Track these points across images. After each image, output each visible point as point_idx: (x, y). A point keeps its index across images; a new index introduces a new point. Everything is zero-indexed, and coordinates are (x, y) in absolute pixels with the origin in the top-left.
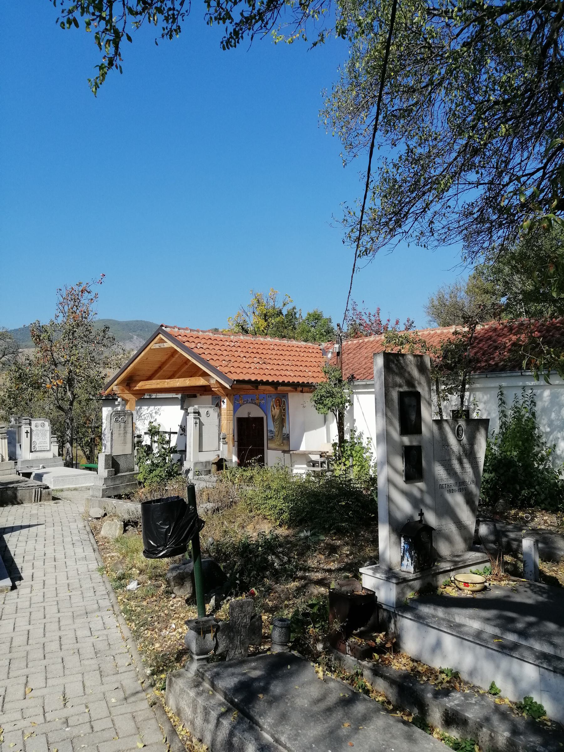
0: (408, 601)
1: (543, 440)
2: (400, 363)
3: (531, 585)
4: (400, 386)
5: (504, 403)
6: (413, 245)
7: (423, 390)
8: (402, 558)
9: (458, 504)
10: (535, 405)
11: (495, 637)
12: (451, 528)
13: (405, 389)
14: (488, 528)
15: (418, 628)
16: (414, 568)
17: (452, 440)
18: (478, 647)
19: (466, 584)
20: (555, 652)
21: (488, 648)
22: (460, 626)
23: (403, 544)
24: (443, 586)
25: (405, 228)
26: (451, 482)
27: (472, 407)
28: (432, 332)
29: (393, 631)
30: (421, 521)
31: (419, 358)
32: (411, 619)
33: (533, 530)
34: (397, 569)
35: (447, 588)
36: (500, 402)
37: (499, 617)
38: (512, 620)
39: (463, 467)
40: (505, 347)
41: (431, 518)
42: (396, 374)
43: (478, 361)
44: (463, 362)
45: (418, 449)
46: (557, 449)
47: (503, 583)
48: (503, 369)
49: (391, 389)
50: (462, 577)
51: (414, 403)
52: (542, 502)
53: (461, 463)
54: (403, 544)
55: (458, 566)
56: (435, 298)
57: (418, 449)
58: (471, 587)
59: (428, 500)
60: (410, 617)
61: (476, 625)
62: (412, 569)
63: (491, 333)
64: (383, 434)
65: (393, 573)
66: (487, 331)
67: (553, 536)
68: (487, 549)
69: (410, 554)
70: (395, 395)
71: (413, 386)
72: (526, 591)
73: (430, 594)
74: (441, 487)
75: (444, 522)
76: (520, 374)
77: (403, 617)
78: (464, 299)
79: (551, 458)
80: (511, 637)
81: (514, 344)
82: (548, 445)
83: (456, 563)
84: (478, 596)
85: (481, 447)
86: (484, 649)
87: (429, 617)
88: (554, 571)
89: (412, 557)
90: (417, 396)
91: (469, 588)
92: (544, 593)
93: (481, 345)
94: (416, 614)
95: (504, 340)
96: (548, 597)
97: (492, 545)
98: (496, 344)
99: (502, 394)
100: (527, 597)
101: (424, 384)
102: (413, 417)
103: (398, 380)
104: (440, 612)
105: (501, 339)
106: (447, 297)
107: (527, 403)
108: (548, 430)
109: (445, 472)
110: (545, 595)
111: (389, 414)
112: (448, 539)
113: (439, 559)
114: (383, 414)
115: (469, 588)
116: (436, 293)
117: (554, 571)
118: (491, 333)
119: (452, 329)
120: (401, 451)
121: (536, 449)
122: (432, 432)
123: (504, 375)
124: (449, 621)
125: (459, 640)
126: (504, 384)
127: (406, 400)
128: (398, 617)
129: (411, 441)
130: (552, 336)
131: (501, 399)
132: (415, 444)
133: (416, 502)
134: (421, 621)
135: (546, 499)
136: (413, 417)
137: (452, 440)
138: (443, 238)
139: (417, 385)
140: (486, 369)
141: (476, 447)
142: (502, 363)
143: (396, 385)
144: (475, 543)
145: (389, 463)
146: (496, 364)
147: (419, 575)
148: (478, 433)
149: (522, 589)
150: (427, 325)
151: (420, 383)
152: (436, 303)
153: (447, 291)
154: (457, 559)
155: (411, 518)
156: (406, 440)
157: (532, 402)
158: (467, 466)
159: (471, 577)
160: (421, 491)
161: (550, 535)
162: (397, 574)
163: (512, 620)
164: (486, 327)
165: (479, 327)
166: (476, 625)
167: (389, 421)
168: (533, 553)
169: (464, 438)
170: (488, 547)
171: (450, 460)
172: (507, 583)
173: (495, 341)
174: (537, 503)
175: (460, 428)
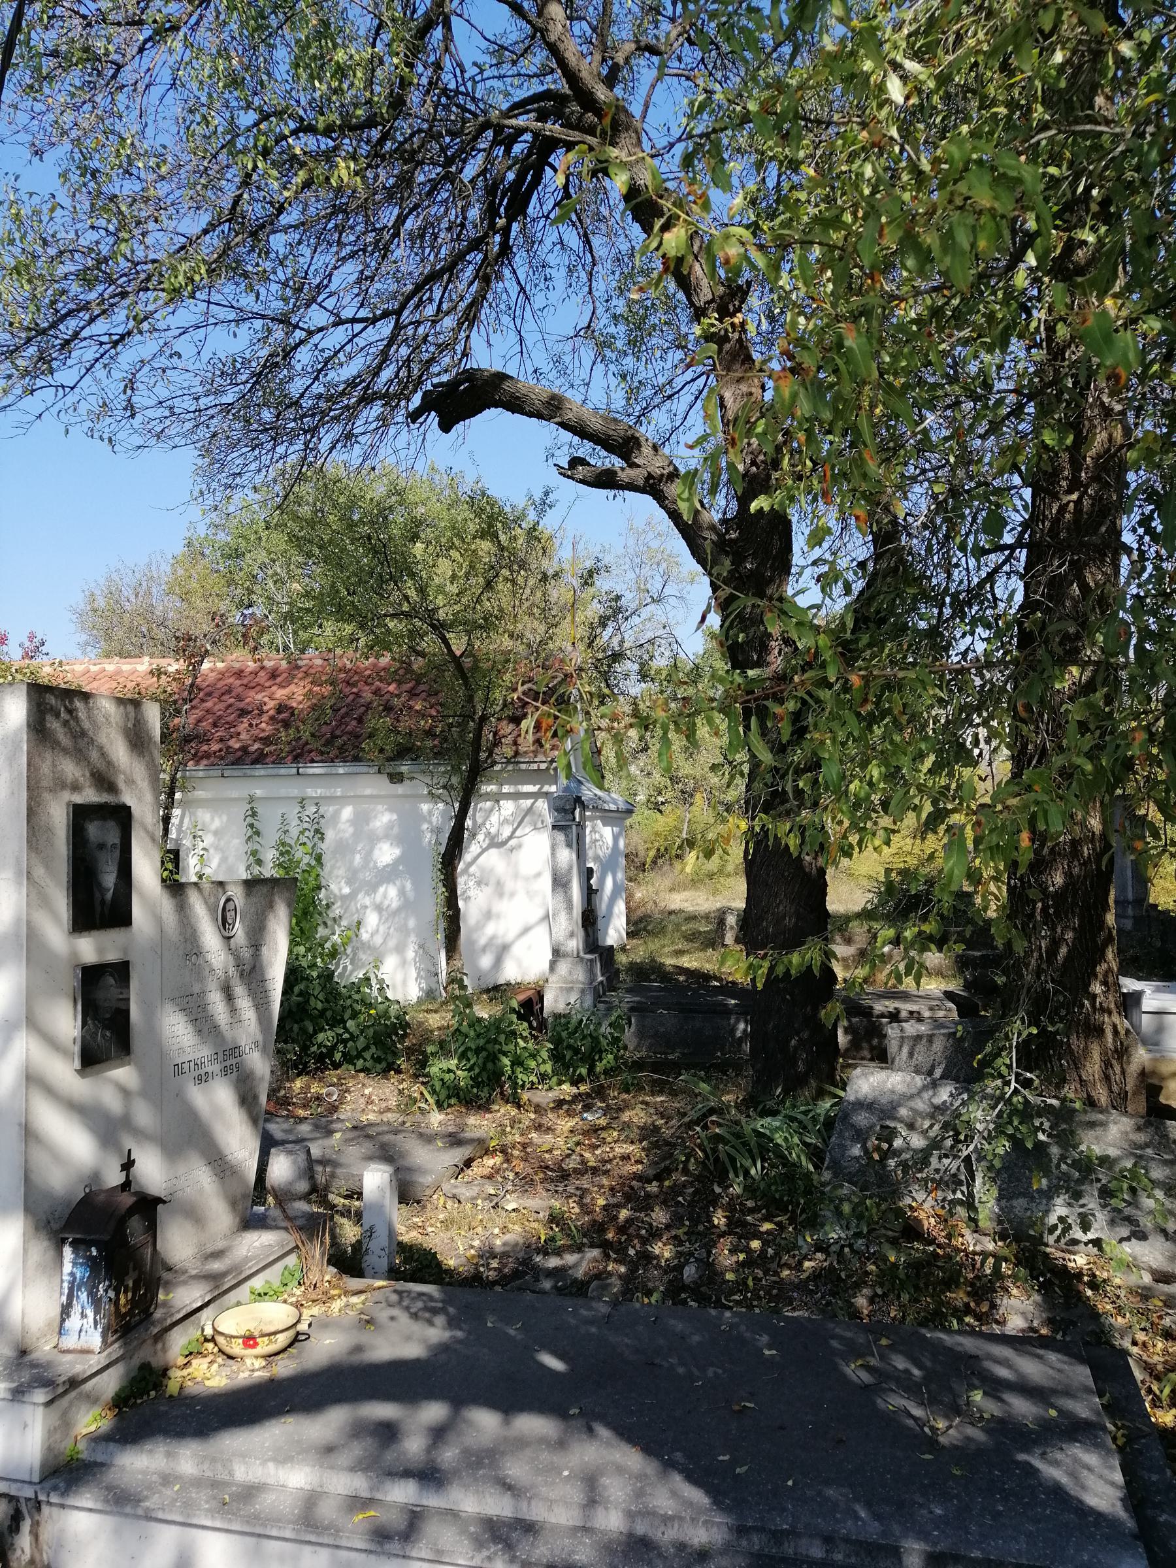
0: (82, 1446)
1: (336, 911)
2: (77, 719)
3: (399, 1293)
4: (76, 788)
5: (258, 833)
6: (77, 432)
7: (140, 799)
8: (66, 1311)
9: (217, 1111)
10: (322, 839)
11: (357, 1503)
12: (200, 1181)
13: (90, 796)
14: (295, 1162)
15: (117, 1532)
16: (104, 1335)
17: (210, 938)
18: (308, 1549)
19: (250, 1340)
20: (516, 1509)
21: (337, 1547)
22: (250, 1492)
23: (68, 1267)
24: (181, 1361)
25: (65, 376)
26: (205, 1052)
27: (187, 842)
28: (94, 669)
29: (26, 1557)
30: (126, 1185)
31: (130, 708)
32: (90, 1510)
33: (355, 1128)
34: (44, 1349)
35: (195, 1362)
36: (250, 833)
37: (359, 1430)
38: (388, 1433)
39: (233, 1010)
40: (261, 712)
41: (152, 1172)
42: (65, 751)
43: (203, 738)
44: (204, 735)
45: (121, 971)
46: (362, 930)
47: (337, 1305)
48: (259, 759)
49: (46, 796)
50: (232, 1321)
51: (113, 837)
52: (359, 1056)
53: (229, 997)
54: (68, 1267)
55: (222, 1287)
56: (97, 592)
57: (121, 971)
58: (265, 1347)
59: (144, 1115)
60: (90, 1505)
61: (297, 1478)
62: (94, 1339)
63: (231, 680)
64: (17, 935)
65: (34, 1365)
66: (222, 674)
67: (401, 1136)
68: (288, 1218)
69: (92, 1294)
70: (58, 816)
71: (112, 788)
72: (392, 1318)
73: (150, 1406)
74: (178, 1070)
75: (181, 1169)
76: (294, 771)
77: (63, 1506)
78: (167, 606)
79: (349, 951)
80: (402, 1493)
81: (281, 708)
82: (344, 923)
83: (214, 1278)
84: (285, 1368)
85: (277, 951)
86: (324, 1553)
87: (149, 1488)
88: (416, 1226)
89: (96, 1302)
90: (122, 816)
91: (259, 1350)
92: (435, 1311)
93: (209, 704)
94: (109, 1488)
95: (259, 697)
96: (452, 1323)
97: (302, 1206)
98: (241, 705)
99: (254, 814)
100: (405, 1338)
101: (144, 784)
102: (109, 879)
103: (70, 769)
104: (186, 1459)
105: (252, 693)
106: (128, 593)
107: (307, 833)
108: (346, 890)
109: (190, 1028)
110: (440, 1320)
111: (39, 872)
112: (194, 1214)
113: (166, 1276)
114: (18, 873)
115: (259, 1350)
116: (102, 581)
117: (416, 1226)
118: (231, 680)
119: (144, 665)
120: (72, 981)
121: (321, 932)
122: (159, 921)
123: (262, 772)
124: (215, 1484)
125: (251, 1541)
126: (259, 793)
127: (93, 830)
128: (45, 1509)
129: (100, 950)
130: (358, 695)
131: (252, 826)
132: (112, 956)
133: (108, 1129)
134: (128, 1510)
135: (367, 1048)
136: (109, 879)
137: (210, 938)
138: (158, 429)
139: (121, 785)
140: (222, 758)
141: (265, 951)
142: (256, 746)
143: (61, 784)
144: (255, 1204)
145: (32, 1022)
146: (244, 749)
147: (116, 1350)
148: (271, 916)
149: (383, 1315)
150: (78, 653)
151: (130, 782)
152: (101, 603)
153: (126, 581)
154: (216, 1266)
155: (96, 1176)
156: (89, 948)
157: (317, 831)
158: (244, 1004)
159: (254, 1313)
160: (125, 1092)
161: (392, 1137)
162: (48, 1365)
163: (388, 1433)
164: (220, 665)
165: (206, 665)
166: (297, 1478)
167: (37, 896)
168: (387, 1202)
169: (239, 930)
170: (291, 1213)
171: (202, 993)
172: (348, 1302)
173: (239, 698)
174: (349, 1059)
175: (230, 906)
